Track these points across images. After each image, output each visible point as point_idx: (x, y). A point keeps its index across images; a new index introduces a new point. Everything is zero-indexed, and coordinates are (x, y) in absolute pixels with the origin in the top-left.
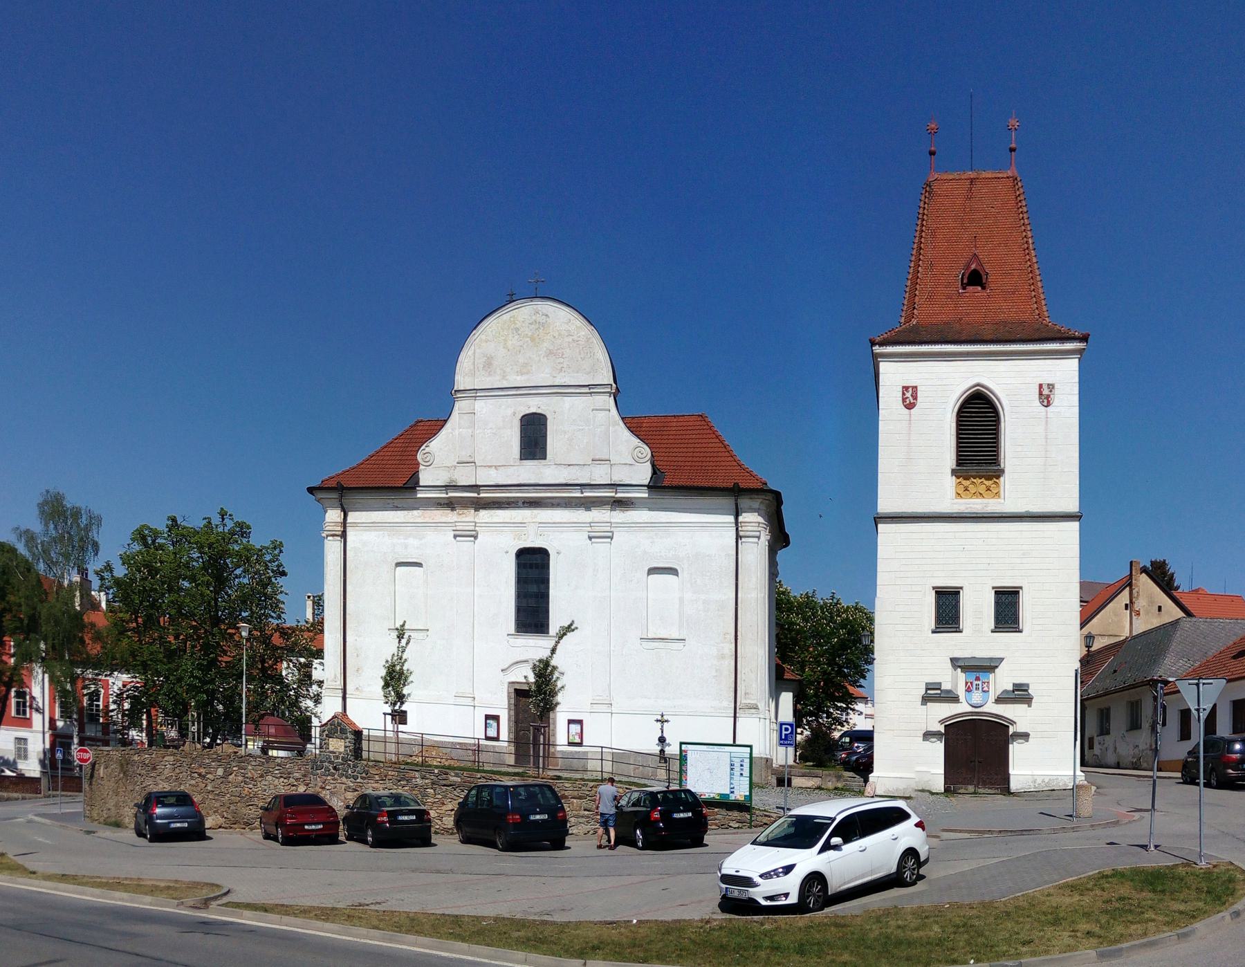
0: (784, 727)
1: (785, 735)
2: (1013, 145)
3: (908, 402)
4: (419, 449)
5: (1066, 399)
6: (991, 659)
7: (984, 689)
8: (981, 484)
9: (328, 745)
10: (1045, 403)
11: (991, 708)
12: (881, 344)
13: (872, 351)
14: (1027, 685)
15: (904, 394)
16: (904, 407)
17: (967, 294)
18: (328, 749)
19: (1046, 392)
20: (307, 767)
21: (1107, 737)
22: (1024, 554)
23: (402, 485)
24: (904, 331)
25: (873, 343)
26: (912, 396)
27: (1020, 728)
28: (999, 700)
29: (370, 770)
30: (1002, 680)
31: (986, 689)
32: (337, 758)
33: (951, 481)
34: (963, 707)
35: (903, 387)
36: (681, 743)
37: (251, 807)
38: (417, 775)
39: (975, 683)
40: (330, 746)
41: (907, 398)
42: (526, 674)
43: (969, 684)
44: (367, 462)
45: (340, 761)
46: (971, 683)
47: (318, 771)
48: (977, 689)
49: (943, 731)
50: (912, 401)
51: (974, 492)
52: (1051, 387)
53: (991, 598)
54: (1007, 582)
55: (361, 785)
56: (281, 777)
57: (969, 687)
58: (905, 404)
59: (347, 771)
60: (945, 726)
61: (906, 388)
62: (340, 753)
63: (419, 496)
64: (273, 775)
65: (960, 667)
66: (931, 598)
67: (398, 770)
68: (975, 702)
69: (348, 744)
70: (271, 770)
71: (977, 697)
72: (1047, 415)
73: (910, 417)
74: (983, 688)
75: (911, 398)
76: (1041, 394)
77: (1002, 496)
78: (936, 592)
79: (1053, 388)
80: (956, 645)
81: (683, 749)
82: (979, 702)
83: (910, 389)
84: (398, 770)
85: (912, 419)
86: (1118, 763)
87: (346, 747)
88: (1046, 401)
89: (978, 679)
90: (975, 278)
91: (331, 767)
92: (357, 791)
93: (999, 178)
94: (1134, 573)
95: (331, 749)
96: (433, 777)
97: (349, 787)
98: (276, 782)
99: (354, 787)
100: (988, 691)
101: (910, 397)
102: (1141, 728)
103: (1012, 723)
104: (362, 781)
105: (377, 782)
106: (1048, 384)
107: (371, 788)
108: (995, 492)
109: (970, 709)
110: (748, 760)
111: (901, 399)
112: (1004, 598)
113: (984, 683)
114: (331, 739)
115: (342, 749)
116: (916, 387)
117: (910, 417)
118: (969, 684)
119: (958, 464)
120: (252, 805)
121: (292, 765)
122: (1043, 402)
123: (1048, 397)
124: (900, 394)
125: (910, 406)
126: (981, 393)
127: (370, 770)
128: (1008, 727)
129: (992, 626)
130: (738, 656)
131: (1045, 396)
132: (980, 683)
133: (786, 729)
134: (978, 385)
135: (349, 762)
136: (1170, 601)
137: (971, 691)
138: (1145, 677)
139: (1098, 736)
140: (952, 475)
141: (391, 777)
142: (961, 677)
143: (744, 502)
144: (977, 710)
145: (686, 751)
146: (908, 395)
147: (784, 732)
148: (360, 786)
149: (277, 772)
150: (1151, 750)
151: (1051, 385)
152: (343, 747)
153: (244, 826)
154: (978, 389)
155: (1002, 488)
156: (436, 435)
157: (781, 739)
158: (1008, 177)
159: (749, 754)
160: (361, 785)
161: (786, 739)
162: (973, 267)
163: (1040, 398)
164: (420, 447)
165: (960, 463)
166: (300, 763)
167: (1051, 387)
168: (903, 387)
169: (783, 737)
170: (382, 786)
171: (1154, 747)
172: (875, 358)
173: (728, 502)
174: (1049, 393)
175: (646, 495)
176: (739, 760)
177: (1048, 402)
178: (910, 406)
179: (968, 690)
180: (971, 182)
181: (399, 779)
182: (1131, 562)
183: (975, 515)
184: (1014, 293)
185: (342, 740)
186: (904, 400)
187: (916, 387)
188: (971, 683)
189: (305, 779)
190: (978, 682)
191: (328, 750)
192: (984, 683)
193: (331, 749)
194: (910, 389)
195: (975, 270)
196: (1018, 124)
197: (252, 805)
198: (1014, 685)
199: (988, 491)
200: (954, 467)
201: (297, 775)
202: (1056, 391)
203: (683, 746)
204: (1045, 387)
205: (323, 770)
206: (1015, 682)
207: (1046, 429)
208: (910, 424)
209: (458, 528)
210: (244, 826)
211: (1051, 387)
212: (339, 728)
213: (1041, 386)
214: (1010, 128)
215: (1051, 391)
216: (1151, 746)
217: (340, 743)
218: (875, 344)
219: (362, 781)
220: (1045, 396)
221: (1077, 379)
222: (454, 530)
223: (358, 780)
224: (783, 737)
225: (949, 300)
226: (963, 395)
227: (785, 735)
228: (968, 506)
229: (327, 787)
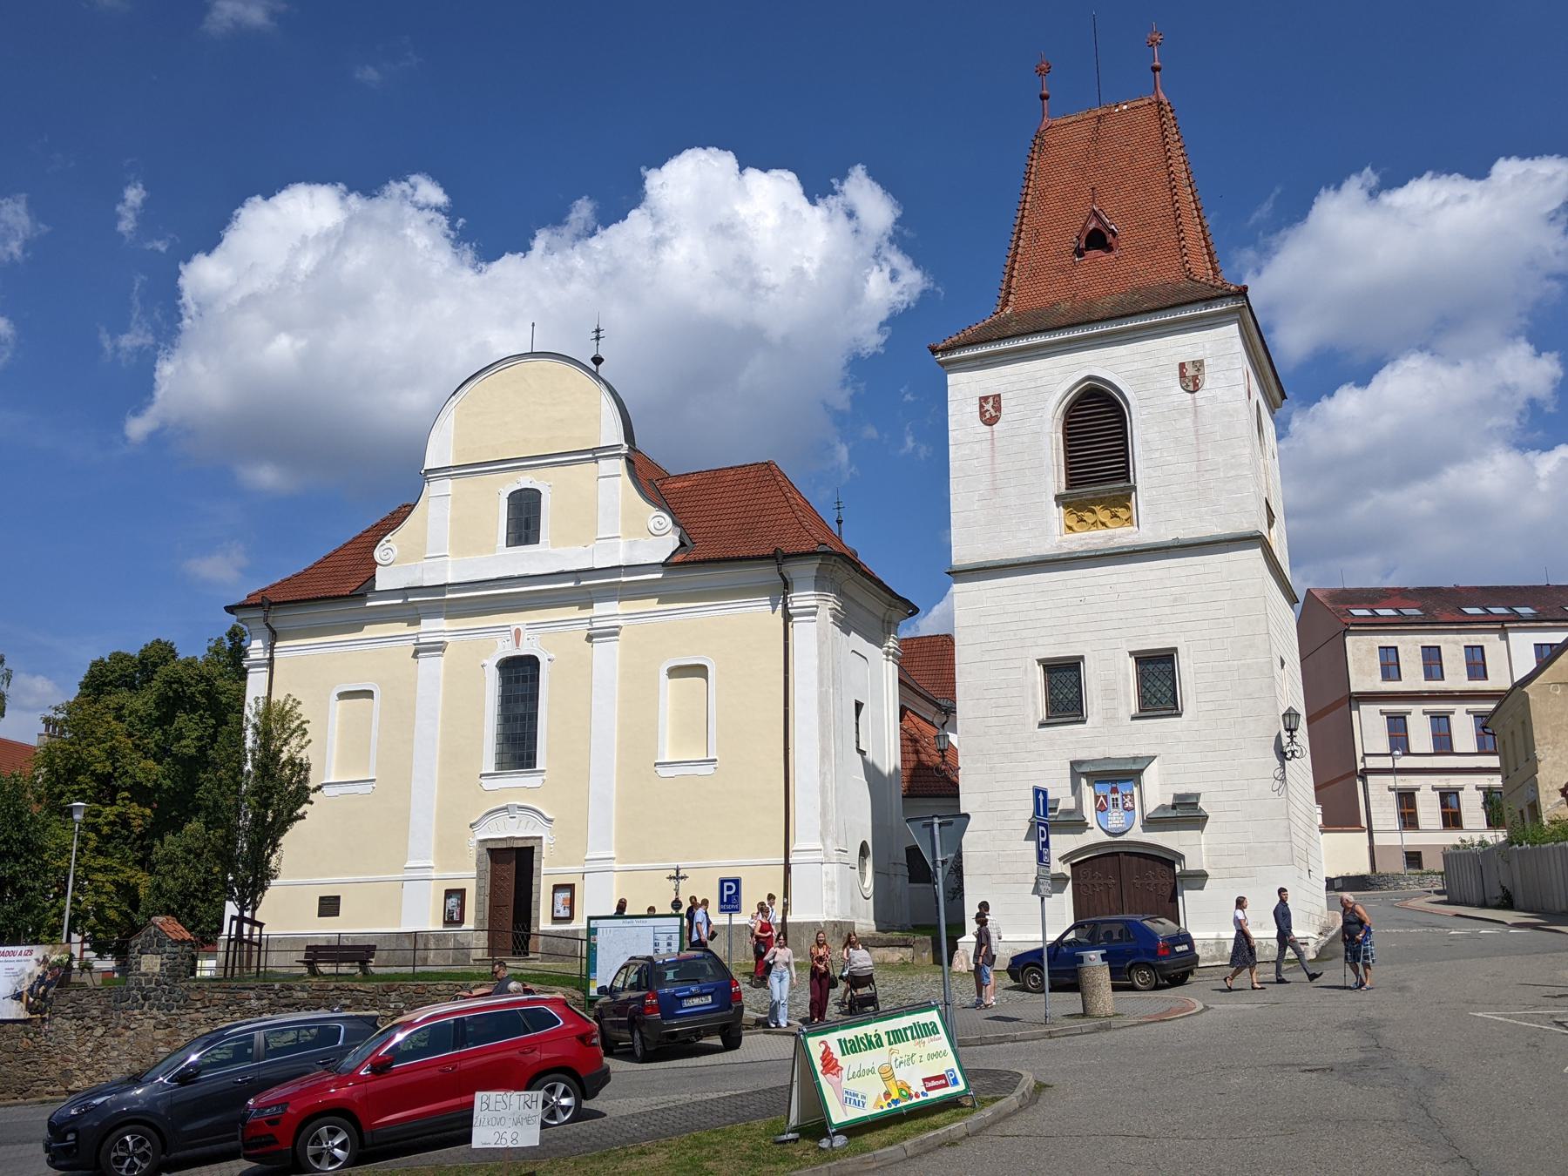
0: (726, 884)
1: (728, 896)
2: (1157, 63)
3: (988, 416)
4: (377, 544)
5: (1222, 377)
6: (1135, 759)
7: (1127, 805)
9: (140, 964)
10: (1191, 388)
11: (1137, 834)
14: (1198, 796)
15: (981, 407)
17: (1086, 262)
18: (139, 970)
19: (1190, 372)
20: (109, 999)
22: (1175, 600)
23: (348, 593)
24: (989, 326)
26: (993, 407)
27: (1191, 864)
28: (1151, 823)
29: (191, 994)
30: (1156, 791)
32: (149, 982)
34: (1094, 836)
35: (981, 398)
36: (590, 918)
37: (28, 1066)
38: (252, 994)
39: (1111, 797)
40: (142, 965)
41: (988, 411)
43: (1102, 798)
44: (319, 566)
45: (153, 985)
46: (1105, 797)
47: (123, 1004)
48: (1115, 805)
51: (1093, 521)
52: (1199, 365)
54: (1154, 642)
55: (176, 1017)
56: (74, 1017)
57: (1102, 804)
59: (160, 1000)
61: (984, 399)
62: (154, 974)
63: (368, 604)
64: (64, 1016)
66: (1039, 673)
67: (227, 990)
69: (165, 961)
70: (62, 1008)
71: (1116, 819)
72: (1195, 403)
73: (993, 435)
74: (1124, 804)
75: (992, 410)
76: (1182, 376)
77: (1135, 523)
78: (1136, 659)
80: (1077, 742)
81: (592, 926)
83: (991, 400)
84: (227, 990)
85: (995, 437)
87: (162, 965)
88: (1191, 384)
89: (1114, 791)
90: (1098, 240)
91: (139, 997)
92: (170, 1026)
93: (1137, 107)
95: (143, 969)
96: (272, 996)
97: (160, 1022)
98: (67, 1025)
99: (167, 1022)
101: (990, 408)
104: (178, 1012)
105: (197, 1010)
106: (1193, 362)
107: (188, 1021)
108: (1125, 518)
110: (678, 936)
111: (978, 413)
114: (144, 956)
115: (157, 969)
116: (999, 395)
117: (993, 435)
118: (1102, 798)
119: (1071, 484)
120: (29, 1063)
121: (90, 998)
122: (1188, 386)
124: (977, 408)
125: (990, 421)
127: (191, 994)
129: (1042, 714)
131: (1191, 378)
132: (1119, 796)
133: (729, 888)
134: (1089, 378)
135: (165, 986)
137: (1106, 809)
140: (1058, 506)
141: (216, 1002)
142: (1088, 792)
143: (794, 570)
145: (596, 929)
146: (988, 407)
147: (726, 893)
148: (175, 1020)
149: (69, 1010)
151: (1198, 361)
152: (159, 965)
153: (16, 1095)
155: (1134, 510)
156: (401, 523)
157: (722, 902)
158: (1150, 104)
159: (678, 927)
160: (176, 1017)
161: (729, 902)
162: (1092, 226)
164: (379, 541)
165: (1071, 485)
166: (100, 994)
167: (1199, 365)
168: (981, 398)
169: (725, 900)
170: (204, 1016)
173: (768, 572)
175: (660, 576)
176: (665, 937)
177: (1196, 385)
178: (990, 421)
179: (1101, 809)
180: (1099, 121)
181: (227, 1003)
183: (1093, 554)
185: (159, 956)
186: (982, 414)
187: (999, 395)
188: (1105, 797)
189: (105, 1017)
190: (1115, 796)
191: (138, 972)
192: (1126, 796)
193: (143, 969)
194: (991, 400)
195: (1094, 229)
196: (1161, 37)
197: (29, 1063)
198: (1176, 796)
199: (1115, 519)
200: (1063, 491)
201: (95, 1012)
203: (592, 922)
205: (130, 1002)
206: (1178, 792)
207: (1195, 422)
208: (993, 444)
209: (421, 641)
210: (16, 1095)
211: (1198, 365)
212: (155, 940)
213: (1182, 366)
214: (1150, 43)
217: (155, 961)
219: (178, 1012)
220: (1191, 378)
222: (415, 644)
223: (173, 1012)
224: (725, 900)
225: (1060, 274)
226: (1064, 398)
227: (728, 896)
228: (1082, 542)
229: (132, 1026)
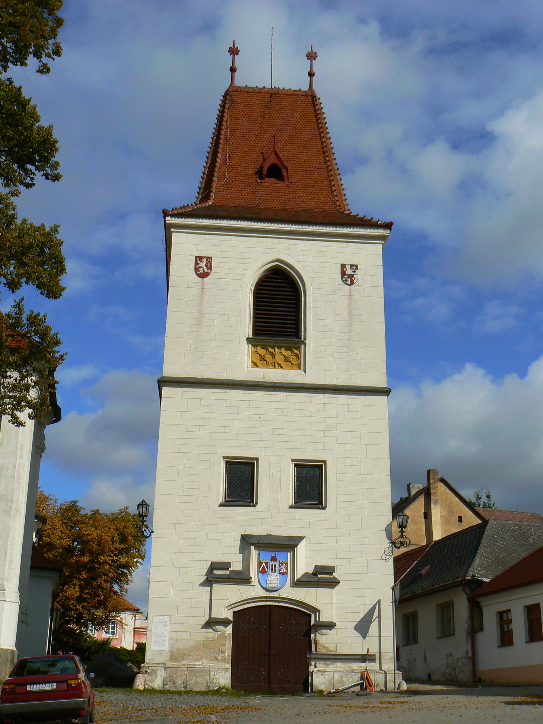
8: (281, 354)
10: (349, 282)
12: (173, 216)
13: (165, 221)
15: (196, 263)
16: (196, 276)
19: (349, 271)
21: (414, 647)
25: (166, 214)
28: (298, 583)
31: (283, 570)
33: (247, 349)
35: (196, 257)
42: (44, 77)
43: (264, 564)
46: (267, 564)
48: (273, 570)
49: (231, 619)
50: (206, 270)
53: (290, 471)
58: (198, 273)
60: (234, 613)
61: (199, 259)
65: (253, 544)
68: (270, 585)
71: (273, 580)
74: (280, 570)
75: (205, 268)
76: (343, 274)
79: (357, 268)
82: (275, 585)
83: (205, 260)
86: (429, 676)
88: (349, 280)
89: (274, 559)
94: (431, 482)
100: (286, 573)
102: (454, 634)
103: (316, 611)
109: (264, 593)
112: (304, 471)
113: (282, 564)
116: (211, 258)
118: (264, 564)
123: (351, 276)
124: (193, 263)
125: (203, 275)
126: (281, 270)
128: (310, 615)
130: (165, 244)
132: (276, 563)
136: (470, 512)
138: (457, 578)
139: (403, 646)
144: (272, 594)
146: (203, 264)
150: (467, 658)
154: (277, 265)
163: (342, 277)
167: (354, 267)
168: (196, 257)
171: (470, 654)
172: (168, 229)
174: (352, 273)
182: (429, 472)
184: (313, 187)
186: (197, 269)
187: (211, 258)
188: (267, 564)
192: (282, 564)
194: (205, 260)
202: (360, 272)
204: (348, 267)
213: (343, 266)
215: (354, 272)
216: (467, 653)
218: (168, 216)
221: (381, 262)
